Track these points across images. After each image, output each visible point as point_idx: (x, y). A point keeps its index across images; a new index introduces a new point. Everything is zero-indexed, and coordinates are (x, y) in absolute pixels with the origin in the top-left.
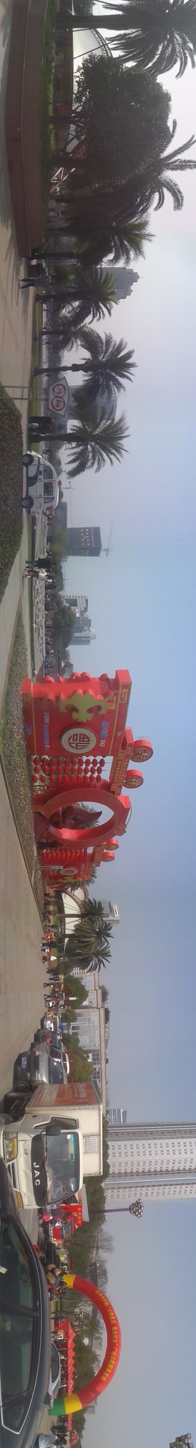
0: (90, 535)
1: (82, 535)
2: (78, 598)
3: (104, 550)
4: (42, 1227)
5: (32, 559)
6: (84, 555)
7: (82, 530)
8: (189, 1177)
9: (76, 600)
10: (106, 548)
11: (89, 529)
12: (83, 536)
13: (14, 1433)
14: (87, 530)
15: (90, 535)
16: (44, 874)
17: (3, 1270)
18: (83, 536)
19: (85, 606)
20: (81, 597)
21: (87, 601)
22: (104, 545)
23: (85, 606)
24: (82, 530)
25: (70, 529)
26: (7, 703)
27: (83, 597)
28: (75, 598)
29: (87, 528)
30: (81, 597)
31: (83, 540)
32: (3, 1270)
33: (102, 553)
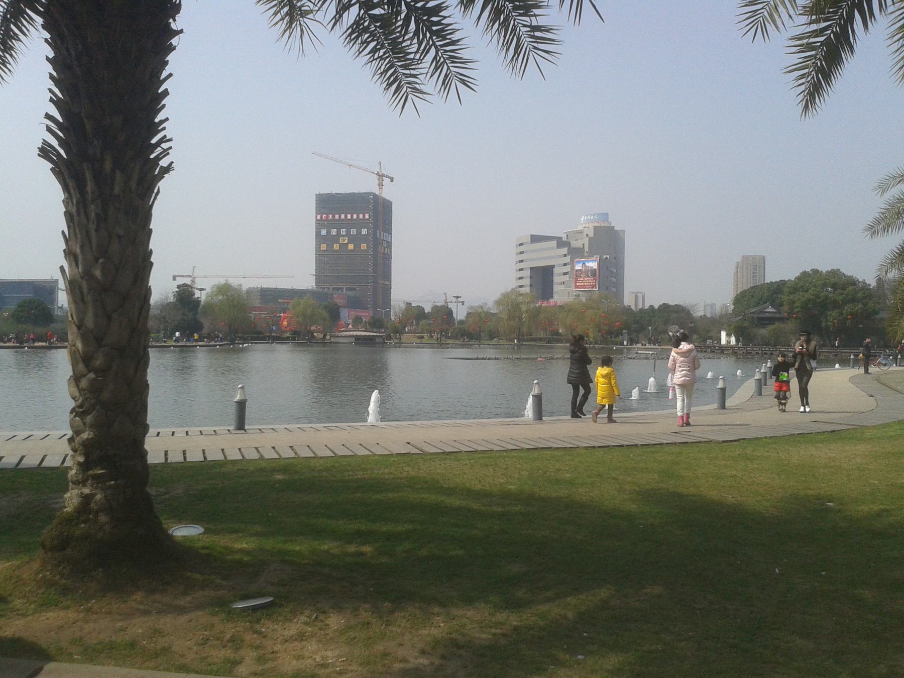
0: (339, 224)
1: (336, 247)
2: (527, 265)
3: (381, 185)
4: (804, 375)
5: (166, 461)
6: (389, 245)
7: (324, 247)
8: (883, 2)
9: (531, 268)
10: (375, 179)
11: (320, 224)
12: (341, 245)
13: (37, 7)
14: (324, 232)
15: (339, 224)
16: (697, 351)
17: (856, 1)
18: (341, 245)
19: (554, 243)
20: (521, 257)
21: (535, 239)
22: (365, 184)
23: (554, 243)
24: (324, 247)
25: (319, 278)
26: (210, 673)
27: (522, 249)
28: (527, 273)
29: (318, 233)
30: (521, 257)
31: (351, 247)
32: (856, 1)
33: (387, 193)
